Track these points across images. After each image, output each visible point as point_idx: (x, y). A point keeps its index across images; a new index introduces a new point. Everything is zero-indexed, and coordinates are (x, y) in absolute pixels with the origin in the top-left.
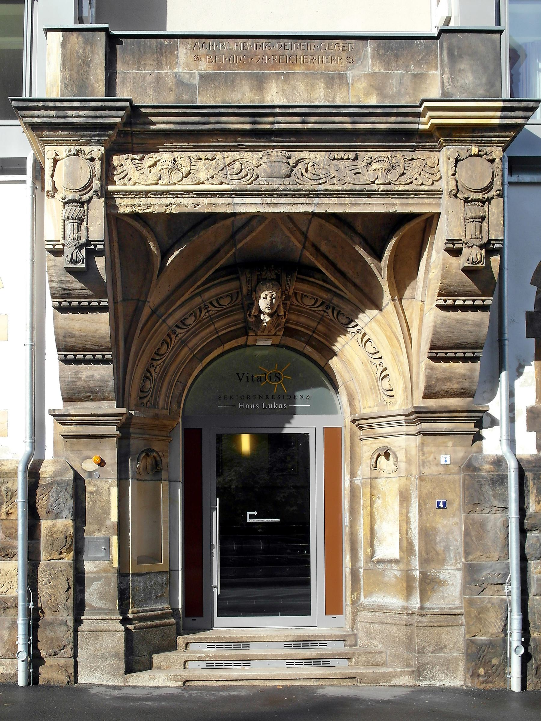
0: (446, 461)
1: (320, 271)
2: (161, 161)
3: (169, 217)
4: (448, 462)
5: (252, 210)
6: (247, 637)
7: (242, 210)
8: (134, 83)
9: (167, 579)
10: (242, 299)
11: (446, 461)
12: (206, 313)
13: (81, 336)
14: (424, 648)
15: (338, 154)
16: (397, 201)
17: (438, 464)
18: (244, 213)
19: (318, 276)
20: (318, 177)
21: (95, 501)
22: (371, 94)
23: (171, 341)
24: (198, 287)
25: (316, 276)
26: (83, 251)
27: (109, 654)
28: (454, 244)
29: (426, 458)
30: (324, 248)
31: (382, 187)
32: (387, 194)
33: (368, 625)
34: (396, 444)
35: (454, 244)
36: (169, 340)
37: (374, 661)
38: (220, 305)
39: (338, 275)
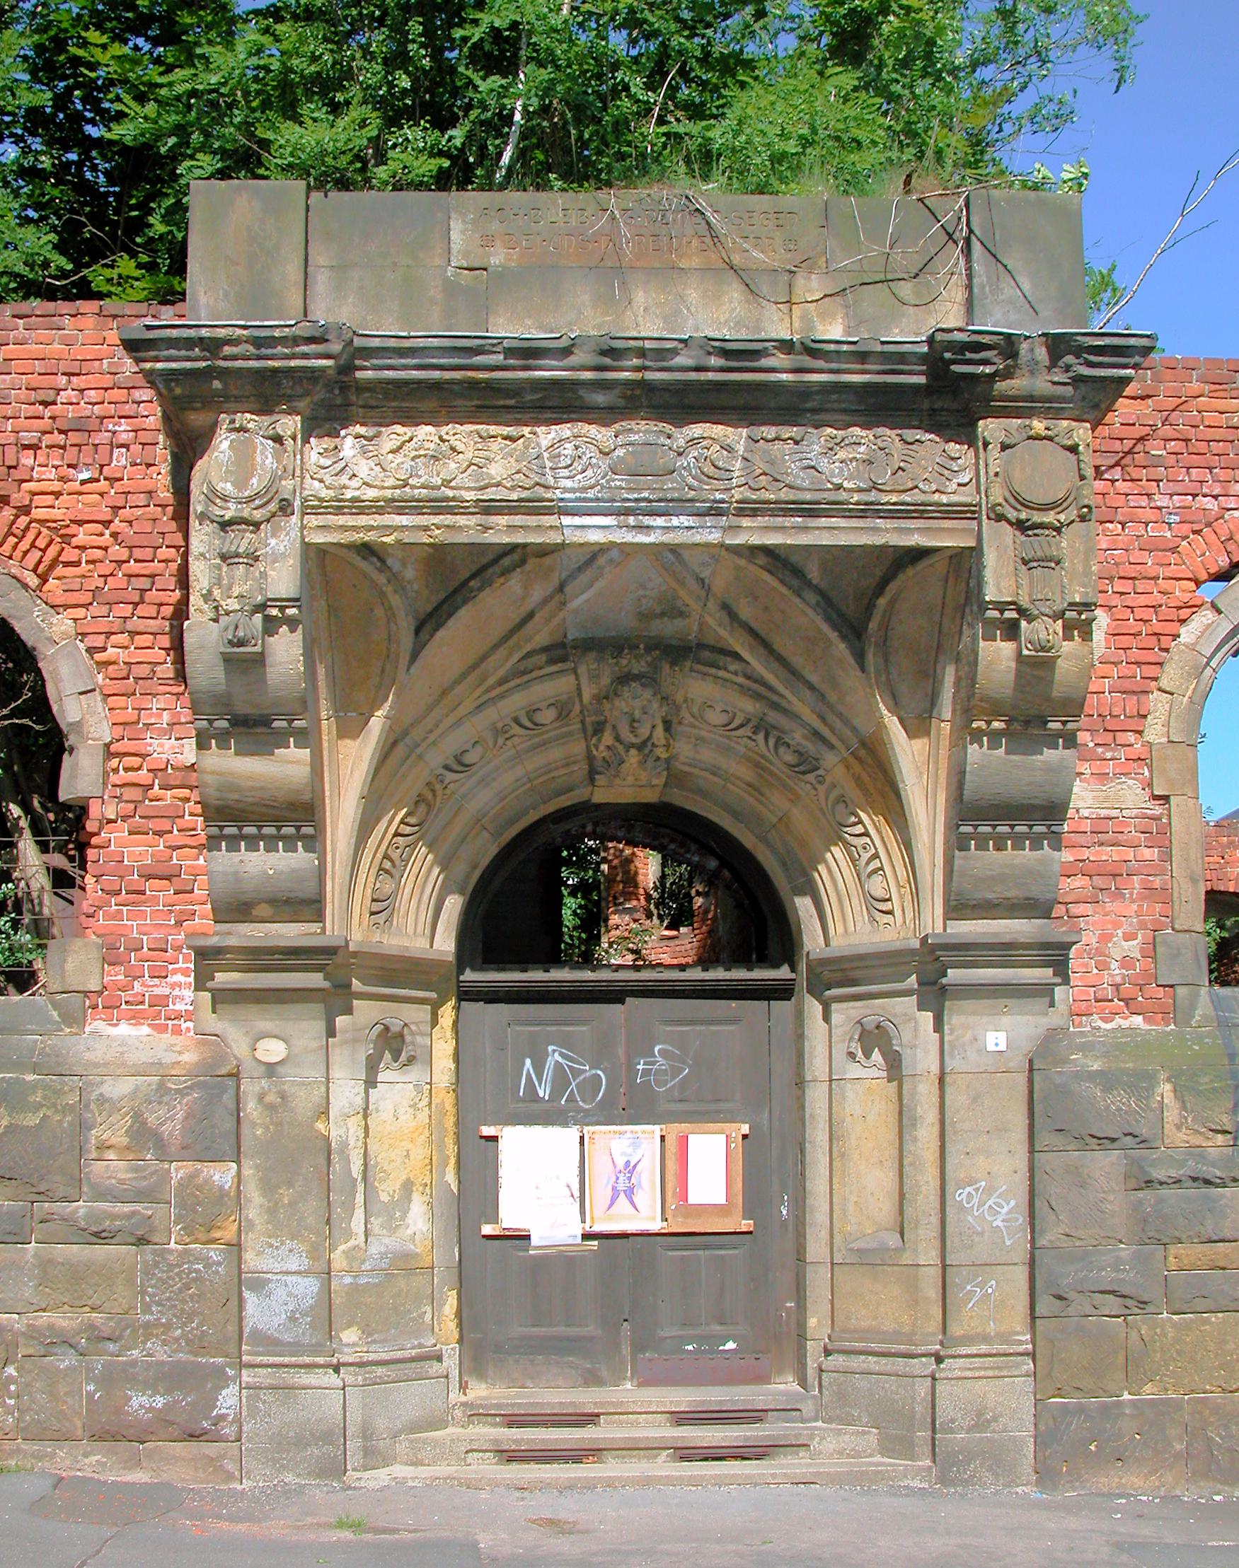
0: (997, 1045)
1: (736, 656)
2: (415, 440)
3: (431, 550)
4: (1003, 1047)
5: (595, 537)
6: (595, 1403)
7: (579, 537)
8: (361, 288)
9: (286, 378)
10: (581, 712)
11: (997, 1045)
12: (915, 123)
13: (253, 788)
14: (952, 1421)
15: (769, 431)
16: (889, 524)
17: (983, 1051)
18: (581, 545)
19: (734, 666)
20: (727, 475)
21: (281, 1124)
22: (833, 316)
23: (434, 796)
24: (488, 690)
25: (732, 667)
26: (258, 617)
27: (312, 1435)
28: (1002, 612)
29: (957, 1039)
30: (745, 612)
31: (856, 498)
32: (866, 512)
33: (842, 1377)
34: (898, 1010)
35: (1002, 612)
36: (430, 796)
37: (853, 1449)
38: (536, 725)
39: (775, 665)
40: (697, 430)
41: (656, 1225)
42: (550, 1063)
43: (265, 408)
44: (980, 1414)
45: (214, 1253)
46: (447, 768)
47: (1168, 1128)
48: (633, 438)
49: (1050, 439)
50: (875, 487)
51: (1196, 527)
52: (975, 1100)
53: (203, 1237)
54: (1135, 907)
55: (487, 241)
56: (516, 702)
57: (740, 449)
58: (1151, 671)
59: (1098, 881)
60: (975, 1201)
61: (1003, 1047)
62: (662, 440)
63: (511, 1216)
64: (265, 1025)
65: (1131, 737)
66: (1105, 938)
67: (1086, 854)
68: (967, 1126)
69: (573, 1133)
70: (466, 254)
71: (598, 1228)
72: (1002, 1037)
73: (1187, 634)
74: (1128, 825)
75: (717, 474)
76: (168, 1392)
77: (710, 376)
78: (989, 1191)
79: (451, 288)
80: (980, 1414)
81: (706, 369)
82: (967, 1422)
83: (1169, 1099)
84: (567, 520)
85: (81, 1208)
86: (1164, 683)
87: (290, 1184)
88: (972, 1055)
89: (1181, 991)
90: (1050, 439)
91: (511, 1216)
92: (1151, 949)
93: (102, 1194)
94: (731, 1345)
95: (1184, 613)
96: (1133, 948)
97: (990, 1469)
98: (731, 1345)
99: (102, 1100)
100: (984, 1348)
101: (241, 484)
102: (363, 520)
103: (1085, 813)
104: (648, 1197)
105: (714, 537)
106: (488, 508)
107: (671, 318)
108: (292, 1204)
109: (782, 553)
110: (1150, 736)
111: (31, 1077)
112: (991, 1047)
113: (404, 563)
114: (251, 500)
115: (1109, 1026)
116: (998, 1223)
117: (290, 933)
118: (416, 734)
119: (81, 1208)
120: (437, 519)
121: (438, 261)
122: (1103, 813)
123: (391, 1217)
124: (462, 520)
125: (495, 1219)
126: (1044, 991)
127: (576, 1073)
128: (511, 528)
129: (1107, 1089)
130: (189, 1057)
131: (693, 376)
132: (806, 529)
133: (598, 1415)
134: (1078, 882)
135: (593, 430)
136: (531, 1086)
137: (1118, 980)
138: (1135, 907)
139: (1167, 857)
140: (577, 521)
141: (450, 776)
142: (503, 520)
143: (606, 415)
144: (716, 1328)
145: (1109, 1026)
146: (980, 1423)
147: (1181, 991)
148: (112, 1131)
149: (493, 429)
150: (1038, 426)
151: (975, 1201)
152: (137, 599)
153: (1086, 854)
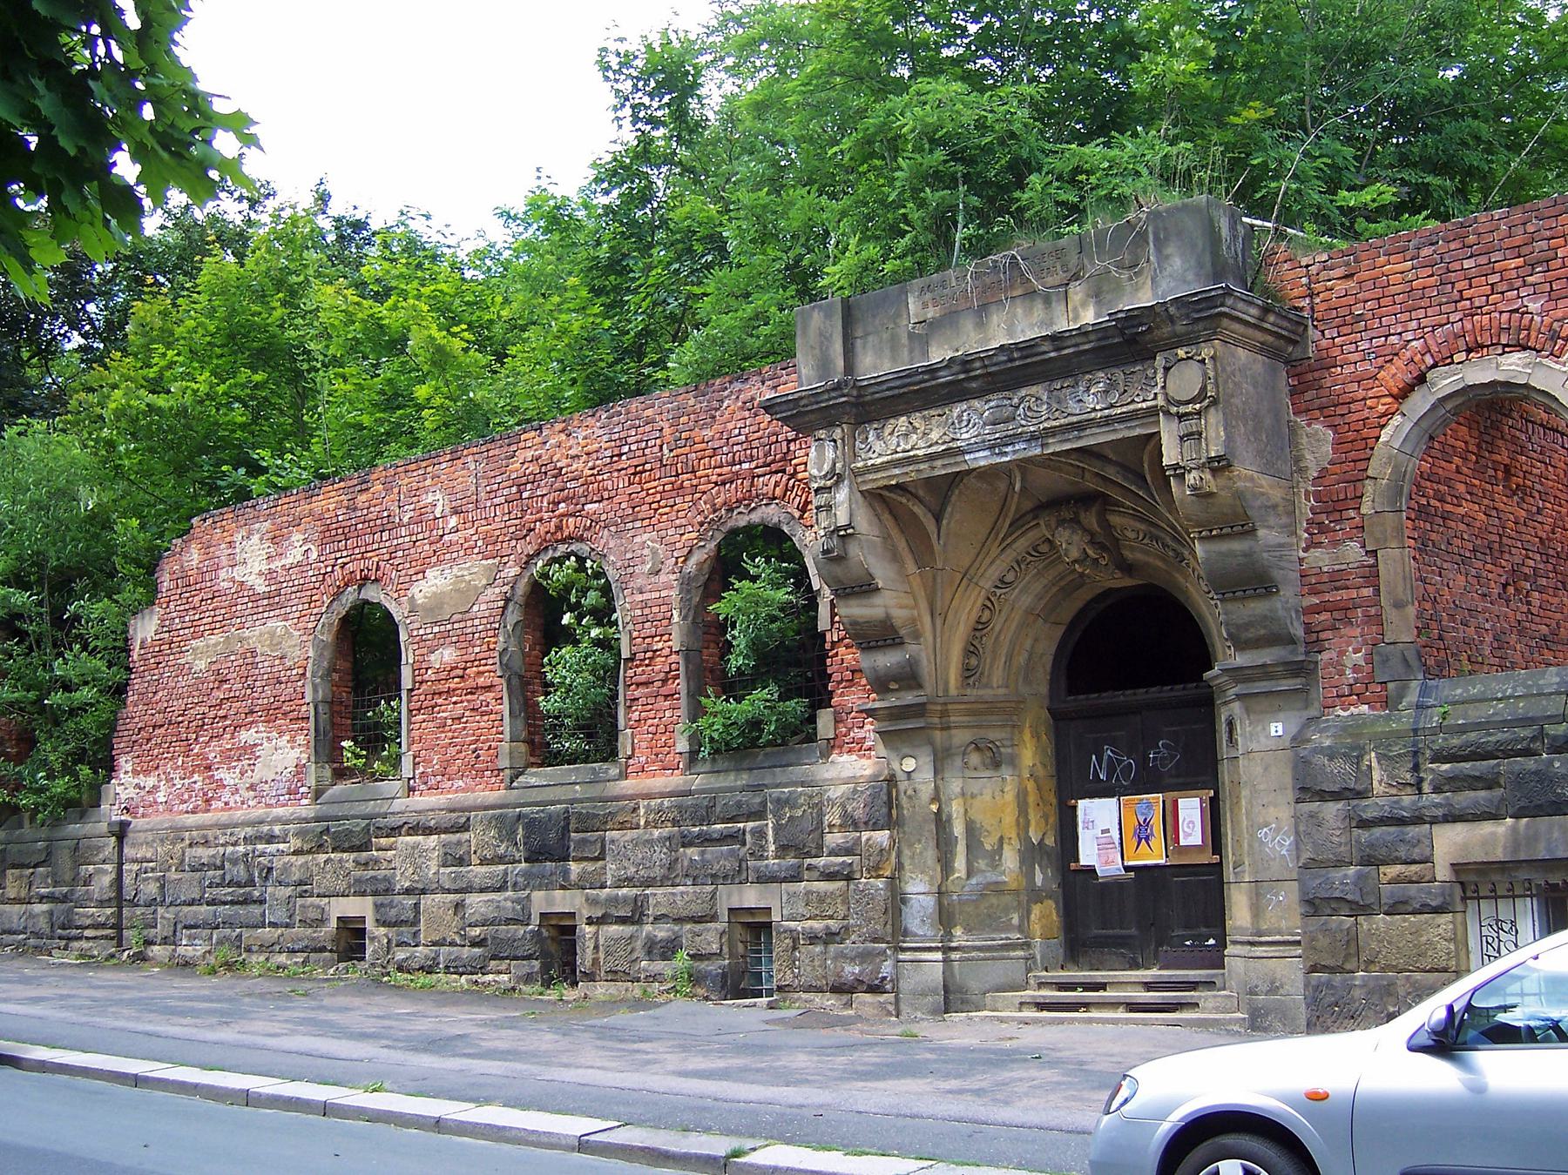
14: (1256, 987)
40: (1023, 392)
41: (1162, 862)
42: (1105, 758)
43: (830, 425)
44: (1272, 983)
45: (880, 883)
46: (996, 587)
47: (1375, 783)
48: (992, 404)
49: (1191, 358)
50: (1112, 406)
51: (1388, 358)
52: (1266, 769)
53: (874, 874)
54: (1359, 630)
55: (925, 305)
56: (1022, 544)
57: (1045, 398)
58: (1361, 465)
59: (1336, 615)
60: (1269, 838)
61: (1280, 733)
62: (1006, 402)
63: (1084, 860)
64: (906, 750)
65: (1352, 513)
66: (1342, 653)
67: (1327, 597)
68: (1262, 787)
69: (1115, 800)
70: (916, 316)
71: (1131, 863)
72: (1280, 726)
73: (1385, 435)
74: (1351, 574)
75: (1035, 415)
76: (861, 964)
77: (1017, 363)
78: (1278, 830)
79: (911, 336)
80: (1272, 983)
81: (1015, 360)
82: (1265, 988)
83: (1374, 761)
84: (967, 457)
85: (821, 862)
86: (1370, 472)
87: (919, 841)
88: (1263, 739)
89: (1391, 686)
90: (1191, 358)
91: (1084, 860)
92: (1369, 659)
93: (832, 853)
94: (1212, 942)
95: (1383, 421)
96: (1359, 657)
97: (1280, 1021)
98: (1212, 942)
99: (829, 799)
100: (1278, 938)
101: (819, 471)
102: (879, 475)
103: (1325, 569)
104: (1158, 841)
105: (1038, 451)
106: (931, 457)
107: (1010, 332)
108: (921, 853)
109: (1095, 449)
110: (1363, 511)
111: (800, 789)
112: (1273, 733)
113: (916, 487)
114: (825, 476)
115: (1346, 714)
116: (1284, 852)
117: (909, 698)
118: (972, 571)
119: (821, 862)
120: (911, 468)
121: (905, 322)
122: (1336, 567)
123: (993, 859)
124: (922, 466)
125: (1077, 860)
126: (1303, 692)
127: (1120, 762)
128: (944, 466)
129: (1331, 759)
130: (868, 772)
131: (1010, 365)
132: (1080, 438)
133: (1105, 984)
134: (1325, 616)
135: (976, 403)
136: (1096, 774)
137: (1352, 681)
138: (1359, 630)
139: (1377, 592)
140: (972, 456)
141: (999, 592)
142: (939, 463)
143: (980, 394)
144: (1204, 930)
145: (1346, 714)
146: (1273, 990)
147: (1391, 686)
148: (833, 817)
149: (932, 412)
150: (1181, 353)
151: (1269, 838)
152: (1458, 298)
153: (1327, 597)
